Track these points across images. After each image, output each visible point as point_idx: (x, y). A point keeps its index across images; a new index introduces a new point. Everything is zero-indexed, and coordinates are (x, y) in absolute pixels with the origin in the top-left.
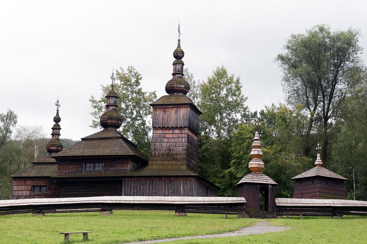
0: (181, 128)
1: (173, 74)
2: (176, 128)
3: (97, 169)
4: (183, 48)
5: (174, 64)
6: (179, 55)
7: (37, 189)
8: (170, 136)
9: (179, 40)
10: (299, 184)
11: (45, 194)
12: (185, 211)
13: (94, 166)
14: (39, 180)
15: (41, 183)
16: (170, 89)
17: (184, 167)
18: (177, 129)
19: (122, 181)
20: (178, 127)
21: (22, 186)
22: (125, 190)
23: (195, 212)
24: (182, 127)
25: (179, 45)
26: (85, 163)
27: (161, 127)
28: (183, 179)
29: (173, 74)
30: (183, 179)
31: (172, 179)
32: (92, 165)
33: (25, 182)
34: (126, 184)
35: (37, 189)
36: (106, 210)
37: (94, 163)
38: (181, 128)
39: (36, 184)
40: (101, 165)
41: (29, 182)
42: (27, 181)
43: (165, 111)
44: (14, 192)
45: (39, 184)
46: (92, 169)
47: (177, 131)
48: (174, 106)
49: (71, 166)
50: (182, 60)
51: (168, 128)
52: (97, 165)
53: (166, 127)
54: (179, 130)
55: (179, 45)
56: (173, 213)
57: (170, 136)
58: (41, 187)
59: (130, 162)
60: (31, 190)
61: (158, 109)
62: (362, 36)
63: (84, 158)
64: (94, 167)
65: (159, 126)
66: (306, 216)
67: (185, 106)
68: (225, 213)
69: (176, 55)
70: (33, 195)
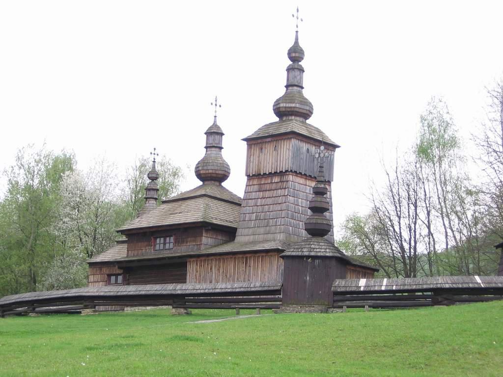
1: (285, 87)
2: (276, 174)
4: (302, 44)
5: (289, 69)
6: (296, 54)
7: (113, 278)
8: (268, 187)
9: (297, 32)
12: (185, 306)
13: (164, 242)
18: (277, 176)
20: (260, 174)
22: (190, 276)
23: (103, 303)
25: (297, 39)
26: (156, 238)
27: (267, 173)
29: (285, 87)
33: (101, 270)
34: (34, 274)
36: (88, 307)
37: (165, 238)
40: (172, 239)
42: (440, 247)
45: (114, 272)
47: (276, 179)
49: (140, 244)
50: (300, 63)
51: (265, 174)
53: (262, 174)
54: (279, 177)
55: (297, 39)
56: (167, 309)
57: (268, 187)
59: (204, 232)
61: (253, 146)
62: (220, 106)
63: (151, 230)
64: (165, 244)
65: (254, 174)
67: (284, 138)
68: (237, 308)
69: (294, 55)
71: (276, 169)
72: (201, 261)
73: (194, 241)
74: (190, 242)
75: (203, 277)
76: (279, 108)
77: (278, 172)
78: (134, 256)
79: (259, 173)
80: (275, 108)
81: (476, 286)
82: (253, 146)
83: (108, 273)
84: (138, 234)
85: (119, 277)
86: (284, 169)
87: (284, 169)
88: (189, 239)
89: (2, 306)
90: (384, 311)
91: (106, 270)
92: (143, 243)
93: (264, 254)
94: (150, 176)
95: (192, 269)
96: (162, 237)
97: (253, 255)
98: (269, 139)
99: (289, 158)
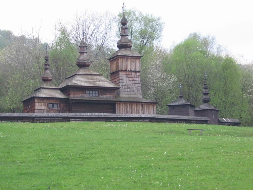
0: (125, 71)
2: (134, 71)
3: (94, 95)
8: (130, 76)
9: (33, 28)
10: (173, 108)
11: (57, 109)
14: (52, 100)
15: (53, 102)
16: (121, 46)
17: (141, 97)
19: (115, 104)
20: (129, 71)
21: (41, 103)
24: (137, 71)
28: (149, 105)
30: (149, 105)
31: (143, 104)
32: (91, 92)
35: (51, 106)
37: (93, 91)
38: (125, 71)
39: (50, 102)
41: (45, 101)
43: (126, 60)
44: (37, 106)
46: (91, 95)
47: (134, 74)
48: (132, 57)
52: (94, 92)
57: (130, 76)
58: (53, 104)
60: (48, 106)
61: (122, 58)
64: (93, 94)
66: (131, 121)
70: (49, 109)
71: (134, 69)
72: (123, 104)
73: (110, 95)
74: (108, 95)
75: (124, 110)
76: (127, 44)
77: (135, 71)
78: (75, 97)
79: (126, 70)
80: (118, 44)
81: (225, 121)
82: (122, 58)
83: (48, 102)
84: (102, 89)
85: (54, 105)
86: (137, 70)
87: (137, 70)
88: (107, 93)
89: (1, 117)
90: (122, 122)
91: (47, 101)
92: (79, 92)
93: (150, 104)
94: (45, 59)
95: (119, 107)
96: (97, 91)
97: (146, 104)
98: (130, 57)
99: (139, 66)
